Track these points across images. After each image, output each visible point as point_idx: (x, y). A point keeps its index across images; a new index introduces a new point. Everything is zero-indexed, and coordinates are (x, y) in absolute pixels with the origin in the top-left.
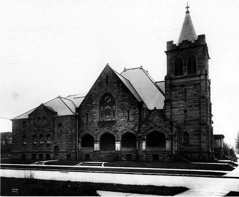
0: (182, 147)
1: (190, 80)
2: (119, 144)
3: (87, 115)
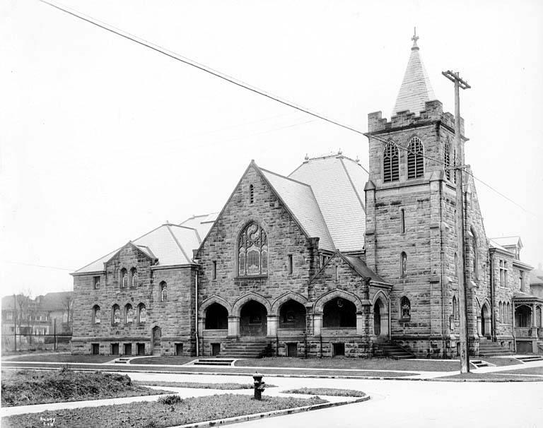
0: (398, 327)
1: (410, 192)
2: (273, 323)
3: (216, 264)
